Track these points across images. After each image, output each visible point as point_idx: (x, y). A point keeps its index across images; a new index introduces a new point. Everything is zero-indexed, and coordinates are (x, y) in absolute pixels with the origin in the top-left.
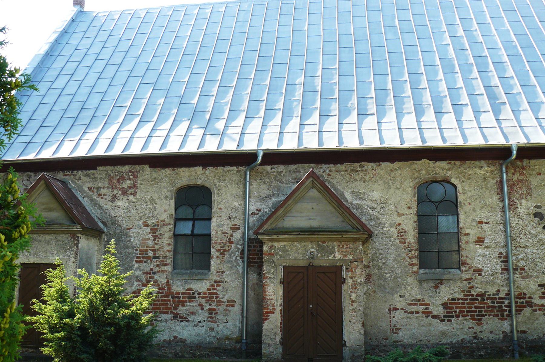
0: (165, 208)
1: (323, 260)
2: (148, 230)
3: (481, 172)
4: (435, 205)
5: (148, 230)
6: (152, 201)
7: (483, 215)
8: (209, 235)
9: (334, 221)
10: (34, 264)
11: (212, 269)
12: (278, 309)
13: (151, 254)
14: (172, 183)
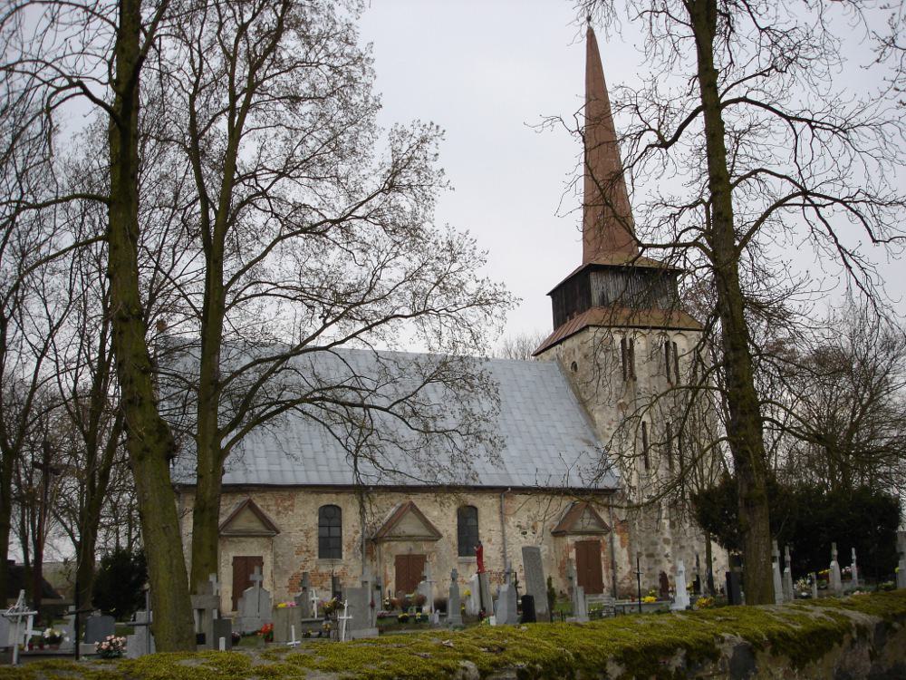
0: (313, 520)
1: (416, 552)
2: (302, 533)
3: (491, 501)
4: (467, 518)
5: (302, 533)
6: (305, 516)
7: (492, 526)
8: (341, 537)
9: (423, 532)
10: (243, 557)
11: (344, 557)
12: (394, 580)
13: (305, 549)
14: (316, 504)
